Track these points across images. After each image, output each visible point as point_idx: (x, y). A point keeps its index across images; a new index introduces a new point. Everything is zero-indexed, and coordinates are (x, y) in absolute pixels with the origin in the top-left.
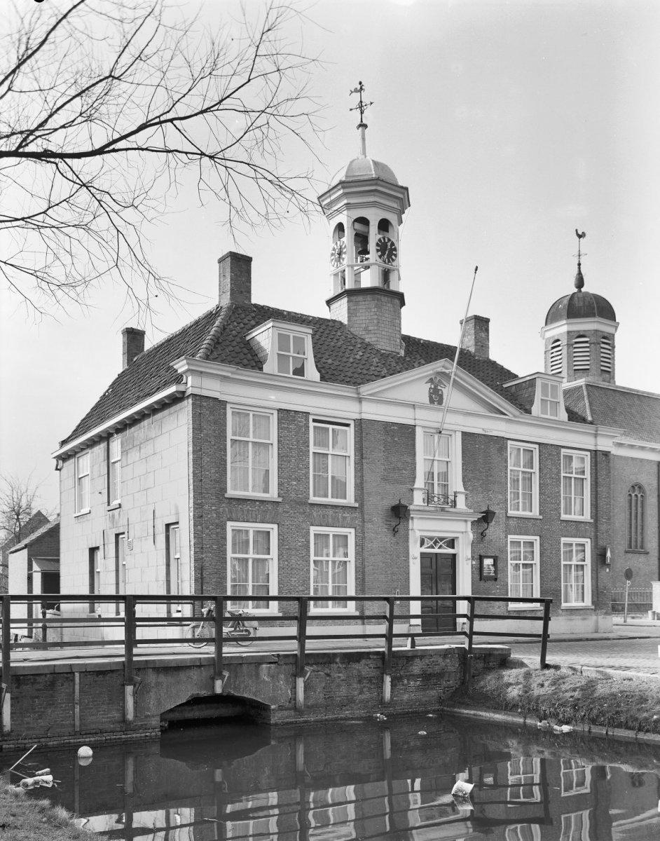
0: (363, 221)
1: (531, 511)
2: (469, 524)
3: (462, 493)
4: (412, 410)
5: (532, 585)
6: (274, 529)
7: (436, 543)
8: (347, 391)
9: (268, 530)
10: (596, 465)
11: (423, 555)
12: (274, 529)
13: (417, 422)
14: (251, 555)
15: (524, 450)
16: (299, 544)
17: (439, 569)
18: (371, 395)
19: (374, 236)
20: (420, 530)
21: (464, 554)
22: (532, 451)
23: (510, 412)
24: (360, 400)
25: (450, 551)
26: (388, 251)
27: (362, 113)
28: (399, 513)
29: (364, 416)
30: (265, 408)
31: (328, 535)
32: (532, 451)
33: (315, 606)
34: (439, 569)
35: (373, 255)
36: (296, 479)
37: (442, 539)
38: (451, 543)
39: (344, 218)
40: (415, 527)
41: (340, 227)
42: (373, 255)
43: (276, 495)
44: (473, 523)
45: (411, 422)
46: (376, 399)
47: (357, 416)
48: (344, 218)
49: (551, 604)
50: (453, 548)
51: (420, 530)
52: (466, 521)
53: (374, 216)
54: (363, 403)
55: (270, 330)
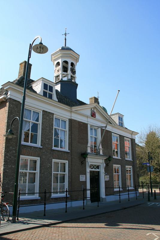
0: (66, 62)
1: (118, 157)
2: (104, 160)
3: (101, 149)
4: (87, 118)
5: (119, 182)
6: (38, 159)
7: (94, 167)
8: (69, 107)
9: (36, 160)
10: (132, 143)
11: (90, 171)
12: (38, 159)
13: (89, 123)
14: (28, 171)
15: (33, 111)
16: (48, 166)
17: (95, 178)
18: (75, 110)
19: (70, 67)
20: (90, 162)
21: (102, 171)
22: (39, 113)
23: (113, 124)
24: (71, 112)
25: (97, 170)
26: (74, 72)
27: (66, 36)
28: (84, 155)
29: (73, 118)
30: (32, 107)
31: (59, 163)
32: (39, 113)
33: (53, 194)
34: (95, 178)
35: (69, 71)
36: (48, 139)
37: (95, 166)
38: (98, 167)
39: (60, 61)
40: (88, 161)
41: (58, 64)
42: (69, 71)
43: (40, 145)
44: (105, 160)
45: (86, 122)
46: (76, 112)
47: (70, 118)
48: (60, 61)
49: (104, 172)
50: (98, 169)
51: (90, 162)
52: (103, 159)
53: (70, 61)
54: (72, 113)
55: (41, 81)
